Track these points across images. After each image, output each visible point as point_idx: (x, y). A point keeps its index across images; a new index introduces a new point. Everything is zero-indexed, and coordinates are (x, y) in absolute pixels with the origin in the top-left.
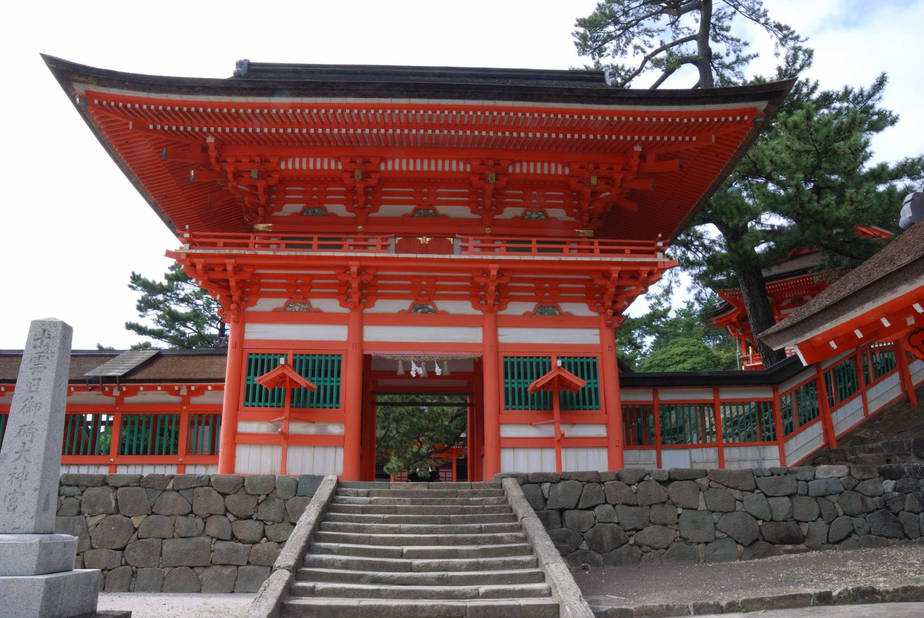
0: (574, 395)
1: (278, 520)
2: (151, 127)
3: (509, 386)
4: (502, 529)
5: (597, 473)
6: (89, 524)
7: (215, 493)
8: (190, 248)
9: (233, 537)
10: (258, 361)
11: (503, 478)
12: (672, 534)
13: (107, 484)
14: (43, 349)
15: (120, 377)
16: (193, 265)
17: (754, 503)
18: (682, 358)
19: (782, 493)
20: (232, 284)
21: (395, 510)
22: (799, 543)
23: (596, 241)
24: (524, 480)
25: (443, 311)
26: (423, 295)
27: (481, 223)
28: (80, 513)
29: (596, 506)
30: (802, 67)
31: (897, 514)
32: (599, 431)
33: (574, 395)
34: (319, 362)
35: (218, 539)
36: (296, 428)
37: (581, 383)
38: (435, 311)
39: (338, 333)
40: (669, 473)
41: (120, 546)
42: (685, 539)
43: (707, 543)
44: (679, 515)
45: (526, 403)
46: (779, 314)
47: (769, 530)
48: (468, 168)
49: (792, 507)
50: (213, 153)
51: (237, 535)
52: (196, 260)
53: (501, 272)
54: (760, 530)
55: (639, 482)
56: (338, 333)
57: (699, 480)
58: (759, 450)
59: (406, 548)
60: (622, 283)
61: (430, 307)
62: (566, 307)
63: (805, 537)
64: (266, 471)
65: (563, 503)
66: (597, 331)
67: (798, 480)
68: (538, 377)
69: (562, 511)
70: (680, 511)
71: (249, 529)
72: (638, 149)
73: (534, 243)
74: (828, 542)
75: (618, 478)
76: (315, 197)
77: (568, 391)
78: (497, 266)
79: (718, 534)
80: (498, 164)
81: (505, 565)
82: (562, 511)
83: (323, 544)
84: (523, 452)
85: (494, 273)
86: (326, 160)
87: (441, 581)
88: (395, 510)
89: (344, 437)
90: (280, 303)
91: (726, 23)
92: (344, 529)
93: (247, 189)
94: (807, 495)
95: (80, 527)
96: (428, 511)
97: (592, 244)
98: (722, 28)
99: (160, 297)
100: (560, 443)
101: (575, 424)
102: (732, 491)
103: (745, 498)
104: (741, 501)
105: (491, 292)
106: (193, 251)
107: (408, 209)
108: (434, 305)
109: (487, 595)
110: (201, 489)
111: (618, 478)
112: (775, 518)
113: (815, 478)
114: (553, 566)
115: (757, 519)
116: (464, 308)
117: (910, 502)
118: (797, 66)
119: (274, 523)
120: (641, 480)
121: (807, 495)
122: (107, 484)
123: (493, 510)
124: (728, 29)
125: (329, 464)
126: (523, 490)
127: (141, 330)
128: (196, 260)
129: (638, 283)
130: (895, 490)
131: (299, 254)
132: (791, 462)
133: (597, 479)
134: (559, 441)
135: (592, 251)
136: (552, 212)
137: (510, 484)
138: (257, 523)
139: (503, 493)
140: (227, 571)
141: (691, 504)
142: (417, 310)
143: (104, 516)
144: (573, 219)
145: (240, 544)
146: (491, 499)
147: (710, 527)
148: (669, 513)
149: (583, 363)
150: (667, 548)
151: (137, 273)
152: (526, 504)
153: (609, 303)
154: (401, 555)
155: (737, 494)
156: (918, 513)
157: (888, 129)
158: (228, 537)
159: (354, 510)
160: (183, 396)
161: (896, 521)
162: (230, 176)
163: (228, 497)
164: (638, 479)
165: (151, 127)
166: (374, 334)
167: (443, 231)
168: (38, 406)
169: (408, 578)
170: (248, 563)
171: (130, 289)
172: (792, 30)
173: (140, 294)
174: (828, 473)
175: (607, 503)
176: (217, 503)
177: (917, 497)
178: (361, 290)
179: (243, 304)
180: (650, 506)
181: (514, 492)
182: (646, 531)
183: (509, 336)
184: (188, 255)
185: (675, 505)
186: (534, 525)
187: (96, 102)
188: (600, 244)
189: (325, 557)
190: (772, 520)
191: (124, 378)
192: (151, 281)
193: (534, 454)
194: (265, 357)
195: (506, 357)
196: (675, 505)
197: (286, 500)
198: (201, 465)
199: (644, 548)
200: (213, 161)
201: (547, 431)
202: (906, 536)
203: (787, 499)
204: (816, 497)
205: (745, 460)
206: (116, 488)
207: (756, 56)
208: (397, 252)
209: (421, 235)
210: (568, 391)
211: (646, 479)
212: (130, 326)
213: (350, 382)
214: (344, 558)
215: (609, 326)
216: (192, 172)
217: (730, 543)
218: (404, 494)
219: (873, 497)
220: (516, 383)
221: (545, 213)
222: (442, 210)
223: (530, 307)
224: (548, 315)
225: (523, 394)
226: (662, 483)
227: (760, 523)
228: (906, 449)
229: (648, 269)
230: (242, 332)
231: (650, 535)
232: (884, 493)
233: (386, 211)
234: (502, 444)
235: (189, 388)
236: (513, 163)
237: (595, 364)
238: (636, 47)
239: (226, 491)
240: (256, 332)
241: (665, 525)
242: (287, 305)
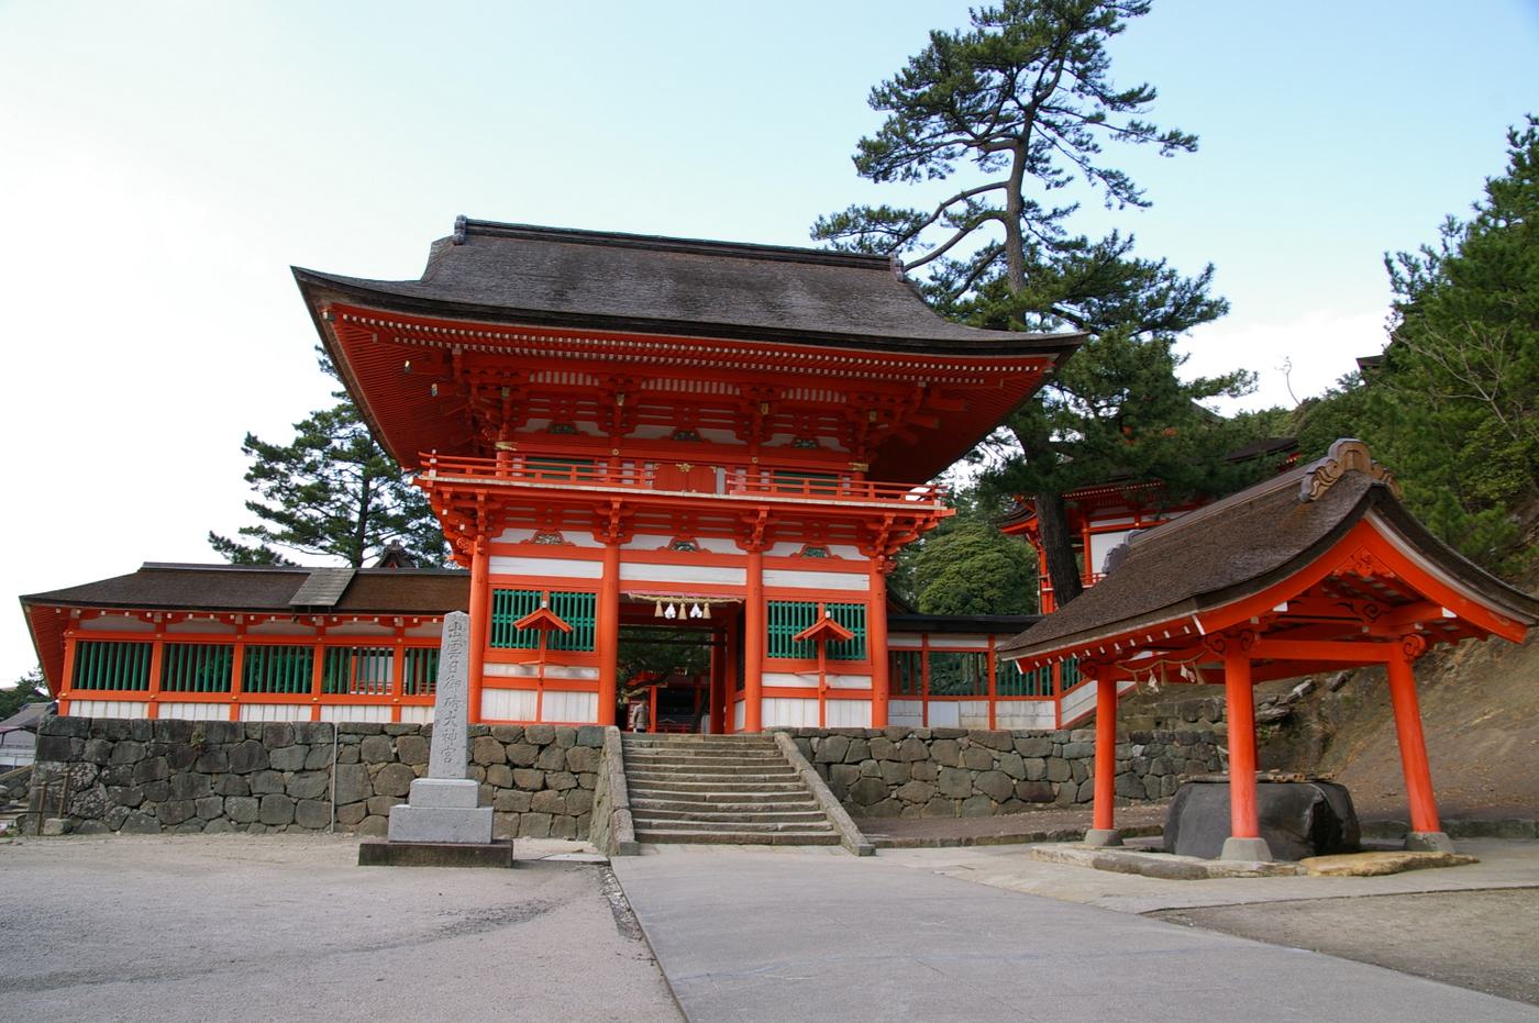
0: (840, 644)
1: (557, 767)
2: (397, 340)
3: (772, 632)
4: (785, 780)
5: (864, 730)
6: (370, 772)
7: (495, 742)
8: (437, 476)
9: (514, 785)
10: (504, 599)
11: (774, 732)
12: (932, 790)
13: (385, 733)
14: (456, 638)
15: (332, 606)
16: (440, 493)
17: (1011, 763)
18: (971, 550)
19: (1038, 755)
20: (481, 514)
21: (684, 761)
22: (1049, 802)
23: (871, 483)
24: (795, 734)
25: (705, 550)
26: (685, 526)
27: (747, 451)
28: (360, 761)
29: (860, 761)
30: (1121, 251)
31: (1142, 777)
32: (864, 683)
33: (840, 644)
34: (576, 601)
35: (500, 787)
36: (551, 672)
37: (847, 633)
38: (697, 549)
39: (593, 570)
40: (932, 732)
41: (403, 794)
42: (943, 795)
43: (963, 799)
44: (939, 772)
45: (790, 651)
46: (1088, 526)
47: (1022, 789)
48: (738, 392)
49: (1046, 768)
50: (457, 365)
51: (518, 783)
52: (443, 489)
53: (770, 513)
54: (1014, 789)
55: (903, 739)
56: (593, 570)
57: (959, 740)
58: (1034, 705)
59: (708, 794)
60: (898, 528)
61: (691, 544)
62: (835, 550)
63: (1055, 797)
64: (514, 716)
65: (831, 757)
66: (867, 577)
67: (1053, 743)
68: (810, 625)
69: (829, 764)
70: (940, 768)
71: (531, 778)
72: (923, 385)
73: (807, 484)
74: (1076, 802)
75: (883, 734)
76: (563, 411)
77: (833, 641)
78: (768, 508)
79: (974, 791)
80: (771, 391)
81: (794, 808)
82: (829, 764)
83: (639, 791)
84: (786, 705)
85: (763, 515)
86: (581, 375)
87: (745, 819)
88: (684, 761)
89: (599, 682)
90: (529, 534)
91: (1046, 153)
92: (646, 777)
93: (489, 402)
94: (1061, 757)
95: (362, 774)
96: (713, 762)
97: (866, 486)
98: (1039, 160)
99: (281, 467)
100: (825, 694)
101: (839, 675)
102: (991, 751)
103: (1002, 758)
104: (999, 761)
105: (753, 531)
106: (441, 479)
107: (668, 430)
108: (695, 542)
109: (784, 829)
110: (481, 739)
111: (883, 734)
112: (1029, 778)
113: (1069, 741)
114: (833, 809)
115: (1012, 778)
116: (727, 547)
117: (1156, 766)
118: (1117, 248)
119: (554, 771)
120: (906, 738)
121: (1061, 757)
122: (385, 733)
123: (771, 762)
124: (1047, 161)
125: (584, 709)
126: (797, 744)
127: (265, 513)
128: (443, 489)
129: (912, 530)
130: (1142, 755)
131: (558, 487)
132: (1068, 719)
133: (864, 735)
134: (824, 693)
135: (866, 495)
136: (826, 441)
137: (782, 737)
138: (538, 772)
139: (776, 747)
140: (510, 818)
141: (950, 762)
142: (677, 548)
143: (385, 764)
144: (847, 450)
145: (521, 792)
146: (767, 752)
147: (968, 784)
148: (931, 769)
149: (849, 611)
150: (926, 803)
151: (253, 435)
152: (802, 758)
153: (882, 549)
154: (705, 799)
155: (995, 754)
156: (1160, 777)
157: (1221, 319)
158: (510, 785)
159: (647, 760)
160: (158, 624)
161: (1141, 784)
162: (474, 390)
163: (508, 747)
164: (902, 736)
165: (397, 340)
166: (632, 572)
167: (708, 457)
168: (458, 683)
169: (720, 817)
170: (531, 810)
171: (244, 453)
172: (1126, 177)
173: (254, 459)
174: (1082, 736)
175: (872, 758)
176: (499, 753)
177: (1162, 761)
178: (618, 524)
179: (488, 534)
180: (913, 762)
181: (789, 747)
182: (909, 785)
183: (775, 579)
184: (435, 483)
185: (936, 762)
186: (813, 778)
187: (345, 317)
188: (876, 487)
189: (646, 801)
190: (1026, 780)
191: (335, 609)
192: (274, 446)
193: (797, 704)
194: (512, 593)
195: (770, 601)
196: (936, 762)
197: (566, 750)
198: (418, 706)
199: (905, 802)
200: (457, 374)
201: (811, 681)
202: (1147, 797)
203: (1042, 760)
204: (1069, 760)
205: (1018, 716)
206: (395, 737)
207: (1076, 207)
208: (655, 488)
209: (682, 462)
210: (833, 641)
211: (910, 736)
212: (252, 506)
213: (604, 621)
214: (662, 801)
215: (879, 572)
216: (407, 364)
217: (985, 800)
218: (685, 746)
219: (1121, 760)
220: (778, 630)
221: (816, 442)
222: (706, 433)
223: (797, 548)
224: (814, 559)
225: (787, 641)
226: (924, 740)
227: (1015, 782)
228: (1176, 712)
229: (924, 516)
230: (486, 566)
231: (911, 790)
232: (1132, 757)
233: (643, 431)
234: (762, 693)
235: (246, 618)
236: (787, 390)
237: (862, 612)
238: (931, 170)
239: (507, 741)
240: (503, 567)
241: (926, 781)
242: (536, 538)
